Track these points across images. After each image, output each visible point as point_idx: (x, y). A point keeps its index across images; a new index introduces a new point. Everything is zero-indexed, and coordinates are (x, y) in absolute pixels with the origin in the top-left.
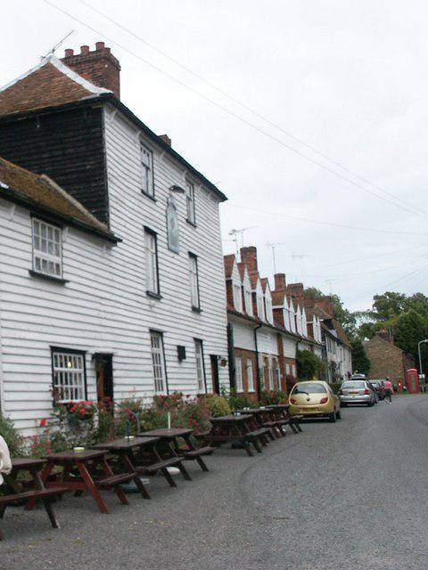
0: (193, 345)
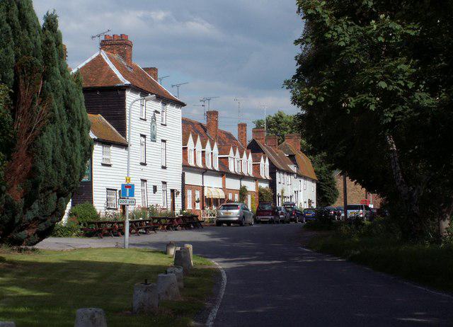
0: (161, 184)
